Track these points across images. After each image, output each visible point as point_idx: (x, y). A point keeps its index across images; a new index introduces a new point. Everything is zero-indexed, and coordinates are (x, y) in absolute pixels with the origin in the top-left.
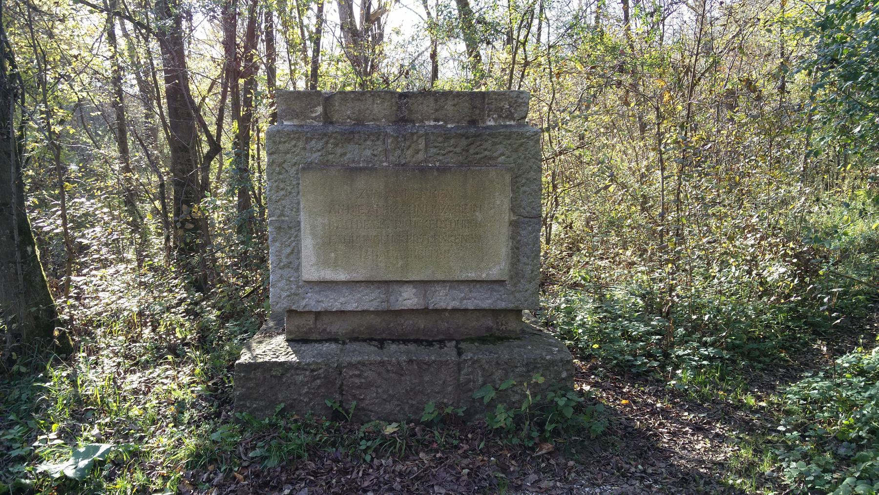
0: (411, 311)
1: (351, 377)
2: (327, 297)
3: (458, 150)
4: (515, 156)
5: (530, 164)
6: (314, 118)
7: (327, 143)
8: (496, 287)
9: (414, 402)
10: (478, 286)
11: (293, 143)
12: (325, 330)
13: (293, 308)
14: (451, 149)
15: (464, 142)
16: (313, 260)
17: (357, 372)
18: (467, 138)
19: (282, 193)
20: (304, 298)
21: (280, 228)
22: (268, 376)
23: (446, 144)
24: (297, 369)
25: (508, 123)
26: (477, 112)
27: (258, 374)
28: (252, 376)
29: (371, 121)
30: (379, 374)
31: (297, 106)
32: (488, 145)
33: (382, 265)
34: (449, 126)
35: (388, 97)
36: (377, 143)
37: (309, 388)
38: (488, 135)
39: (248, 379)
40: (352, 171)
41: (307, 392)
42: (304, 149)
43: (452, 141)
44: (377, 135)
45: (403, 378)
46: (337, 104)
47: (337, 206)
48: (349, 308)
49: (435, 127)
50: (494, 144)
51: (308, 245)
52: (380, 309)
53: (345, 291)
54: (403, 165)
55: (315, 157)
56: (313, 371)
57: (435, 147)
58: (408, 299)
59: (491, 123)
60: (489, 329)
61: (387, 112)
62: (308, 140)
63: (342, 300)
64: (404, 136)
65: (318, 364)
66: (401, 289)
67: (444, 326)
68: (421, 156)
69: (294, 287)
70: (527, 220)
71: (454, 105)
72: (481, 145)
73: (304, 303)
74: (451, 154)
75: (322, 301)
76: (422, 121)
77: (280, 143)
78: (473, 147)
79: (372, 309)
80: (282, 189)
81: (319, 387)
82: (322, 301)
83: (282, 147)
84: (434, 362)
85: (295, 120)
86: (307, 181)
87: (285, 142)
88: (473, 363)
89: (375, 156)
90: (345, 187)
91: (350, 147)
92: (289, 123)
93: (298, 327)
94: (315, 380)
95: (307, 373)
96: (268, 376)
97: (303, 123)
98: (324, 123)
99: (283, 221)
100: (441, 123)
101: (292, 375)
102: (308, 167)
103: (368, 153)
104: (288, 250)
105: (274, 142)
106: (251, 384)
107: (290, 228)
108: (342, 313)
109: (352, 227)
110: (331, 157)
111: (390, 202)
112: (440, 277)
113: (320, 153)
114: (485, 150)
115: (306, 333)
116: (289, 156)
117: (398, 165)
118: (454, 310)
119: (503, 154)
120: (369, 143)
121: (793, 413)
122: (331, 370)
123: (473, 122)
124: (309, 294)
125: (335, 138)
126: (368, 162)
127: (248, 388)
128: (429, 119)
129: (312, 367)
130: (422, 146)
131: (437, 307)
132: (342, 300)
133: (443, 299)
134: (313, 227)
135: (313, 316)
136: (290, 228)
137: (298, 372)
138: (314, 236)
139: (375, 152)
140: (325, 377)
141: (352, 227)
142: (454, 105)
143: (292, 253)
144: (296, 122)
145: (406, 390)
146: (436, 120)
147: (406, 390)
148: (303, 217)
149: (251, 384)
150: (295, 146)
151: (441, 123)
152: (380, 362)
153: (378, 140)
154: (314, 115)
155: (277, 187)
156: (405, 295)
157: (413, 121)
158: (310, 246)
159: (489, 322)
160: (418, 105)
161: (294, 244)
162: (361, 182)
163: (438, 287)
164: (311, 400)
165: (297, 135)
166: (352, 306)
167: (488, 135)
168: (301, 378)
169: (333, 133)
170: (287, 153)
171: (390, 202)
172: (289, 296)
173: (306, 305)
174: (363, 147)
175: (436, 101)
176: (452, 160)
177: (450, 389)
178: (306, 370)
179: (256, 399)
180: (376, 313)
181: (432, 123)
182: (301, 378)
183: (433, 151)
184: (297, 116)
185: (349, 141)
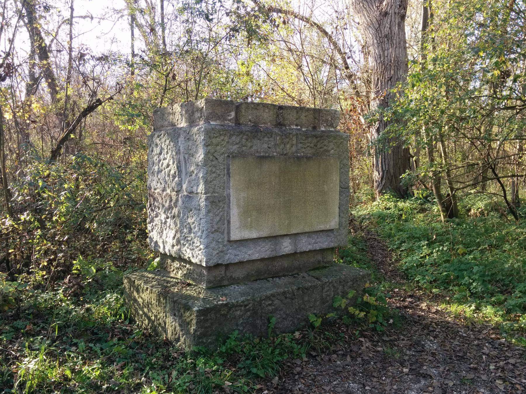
0: (287, 256)
1: (267, 306)
2: (240, 251)
3: (312, 145)
4: (338, 150)
5: (345, 155)
6: (230, 120)
7: (242, 138)
8: (330, 234)
9: (300, 317)
10: (321, 234)
11: (222, 137)
12: (231, 277)
13: (219, 262)
14: (309, 144)
15: (315, 140)
16: (238, 224)
17: (270, 302)
18: (317, 138)
19: (214, 175)
20: (227, 254)
21: (213, 202)
22: (218, 316)
23: (306, 141)
24: (236, 306)
25: (331, 129)
26: (317, 121)
27: (213, 315)
28: (209, 317)
29: (262, 124)
30: (281, 301)
31: (219, 111)
32: (326, 143)
33: (277, 224)
34: (303, 129)
35: (272, 108)
36: (271, 139)
37: (243, 319)
38: (327, 136)
39: (206, 320)
40: (262, 158)
41: (242, 323)
42: (228, 142)
43: (310, 139)
44: (268, 133)
45: (294, 301)
46: (243, 111)
47: (252, 184)
48: (254, 258)
49: (296, 129)
50: (329, 142)
51: (235, 213)
52: (271, 256)
53: (251, 245)
54: (285, 155)
55: (234, 148)
56: (246, 306)
57: (301, 143)
58: (287, 247)
59: (323, 129)
60: (319, 262)
61: (271, 118)
62: (231, 136)
63: (250, 252)
64: (285, 135)
65: (248, 300)
66: (283, 241)
67: (296, 263)
68: (294, 149)
69: (221, 246)
70: (343, 190)
71: (306, 116)
72: (323, 142)
73: (227, 257)
74: (308, 148)
75: (238, 255)
76: (289, 126)
77: (213, 138)
78: (319, 144)
79: (266, 257)
80: (214, 172)
81: (249, 317)
82: (238, 255)
83: (214, 141)
84: (311, 286)
85: (218, 121)
86: (235, 166)
87: (216, 137)
88: (329, 284)
89: (269, 148)
90: (257, 170)
91: (255, 141)
92: (214, 123)
93: (215, 277)
94: (247, 312)
95: (243, 308)
96: (218, 316)
97: (223, 123)
98: (235, 124)
99: (215, 196)
100: (299, 127)
101: (234, 311)
102: (233, 156)
103: (266, 146)
104: (218, 218)
105: (210, 137)
106: (208, 324)
107: (219, 201)
108: (241, 263)
109: (260, 199)
110: (244, 148)
111: (282, 180)
112: (307, 230)
113: (238, 146)
114: (325, 145)
115: (219, 281)
116: (219, 147)
117: (282, 155)
118: (310, 251)
119: (333, 149)
120: (266, 139)
121: (314, 314)
122: (256, 303)
123: (314, 128)
124: (230, 251)
125: (247, 135)
126: (266, 152)
127: (206, 328)
128: (293, 125)
129: (246, 303)
130: (294, 142)
131: (302, 250)
132: (250, 252)
133: (305, 245)
134: (238, 200)
135: (224, 268)
136: (219, 201)
137: (237, 308)
138: (239, 206)
139: (269, 146)
140: (253, 309)
141: (260, 199)
142: (306, 116)
143: (220, 221)
144: (218, 122)
145: (296, 309)
146: (297, 125)
147: (296, 309)
148: (232, 192)
149: (208, 324)
150: (223, 140)
151: (299, 127)
152: (283, 292)
153: (271, 137)
154: (230, 118)
155: (211, 170)
156: (285, 244)
157: (285, 125)
158: (236, 214)
159: (319, 257)
160: (288, 114)
161: (221, 213)
162: (266, 166)
163: (302, 237)
164: (244, 327)
165: (224, 132)
166: (256, 256)
167: (327, 136)
168: (238, 313)
169: (246, 131)
170: (217, 145)
171: (282, 180)
172: (218, 254)
173: (229, 259)
174: (262, 141)
175: (297, 112)
176: (309, 152)
177: (318, 303)
178: (241, 306)
179: (210, 335)
180: (262, 260)
181: (295, 127)
182: (238, 313)
183: (300, 145)
184: (219, 118)
185: (254, 137)
